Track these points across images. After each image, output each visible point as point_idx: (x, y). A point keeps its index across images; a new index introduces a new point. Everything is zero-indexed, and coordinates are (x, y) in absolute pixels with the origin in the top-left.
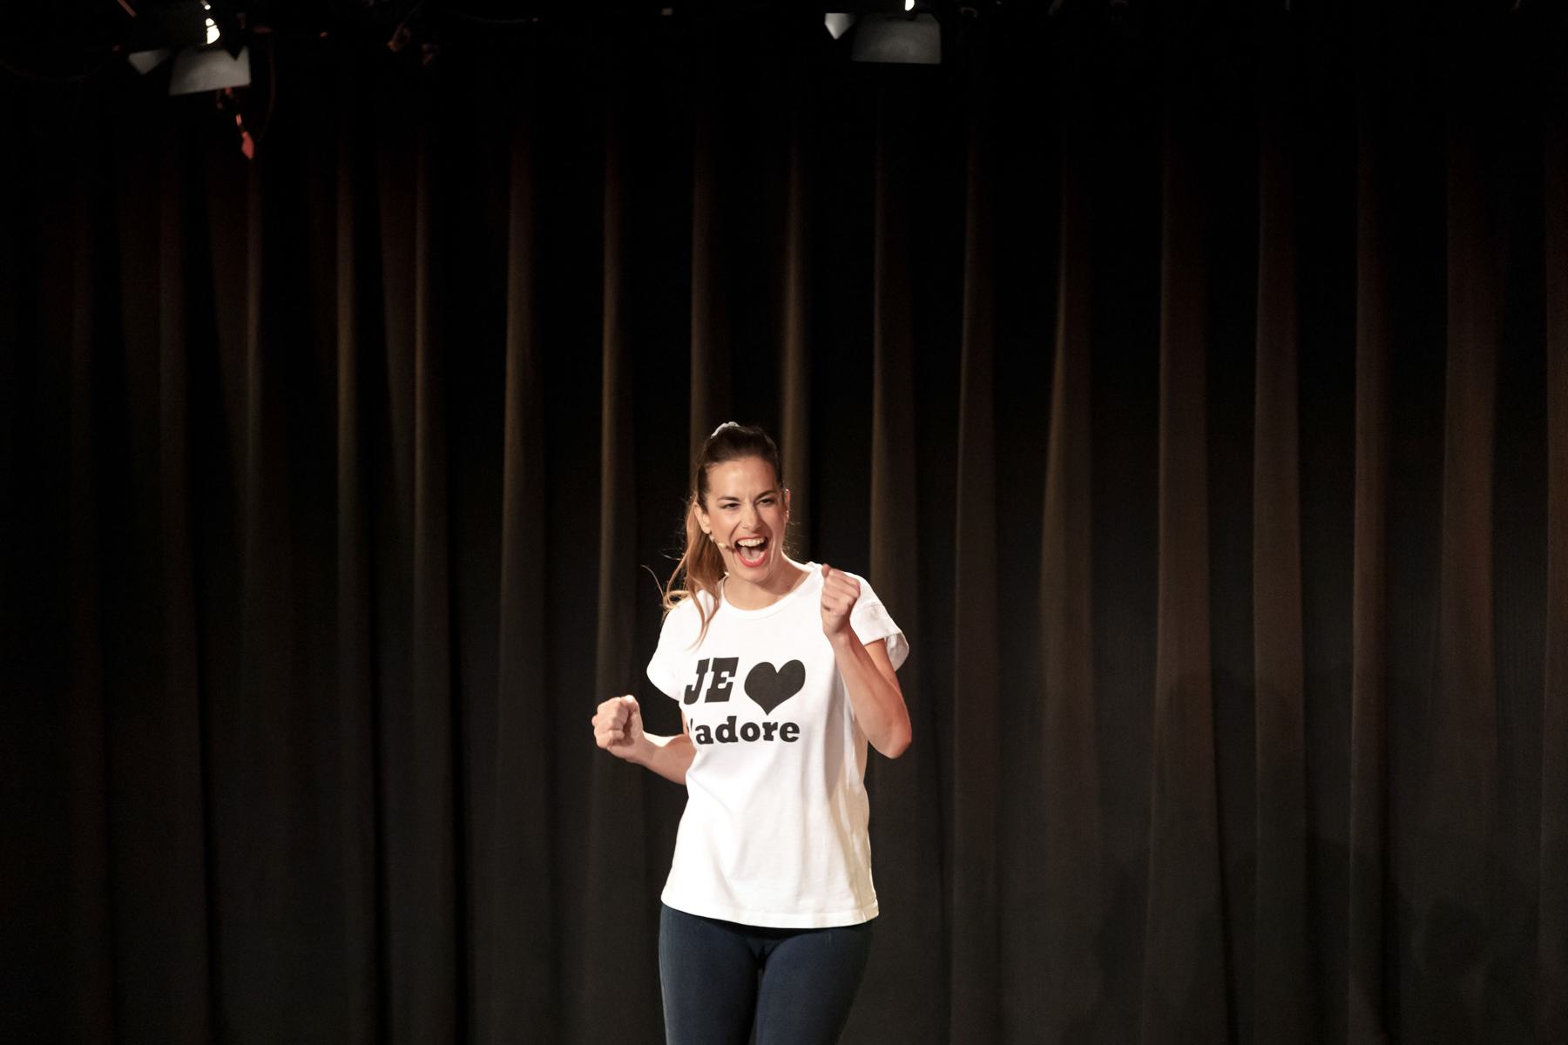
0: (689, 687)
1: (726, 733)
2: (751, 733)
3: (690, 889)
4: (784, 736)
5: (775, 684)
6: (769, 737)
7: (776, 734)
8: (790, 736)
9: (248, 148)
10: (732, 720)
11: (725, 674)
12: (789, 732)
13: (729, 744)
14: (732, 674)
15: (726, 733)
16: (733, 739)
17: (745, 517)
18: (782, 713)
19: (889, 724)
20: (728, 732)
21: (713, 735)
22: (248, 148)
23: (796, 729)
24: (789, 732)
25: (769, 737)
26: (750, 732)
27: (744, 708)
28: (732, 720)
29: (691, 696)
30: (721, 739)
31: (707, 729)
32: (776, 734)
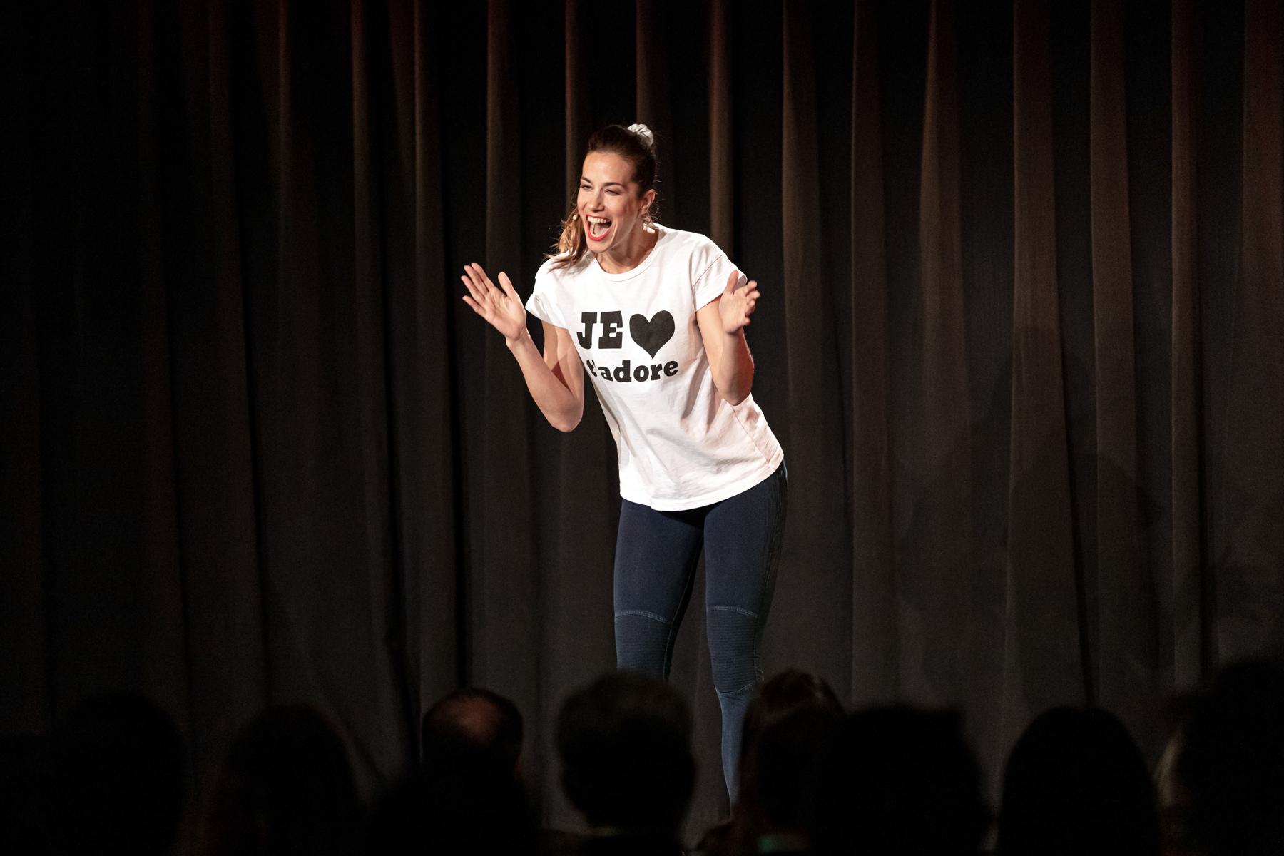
1: (622, 375)
2: (641, 374)
10: (627, 363)
11: (613, 325)
14: (620, 325)
15: (622, 375)
16: (627, 379)
17: (613, 204)
18: (664, 354)
20: (624, 373)
25: (655, 377)
28: (627, 363)
29: (586, 342)
31: (607, 371)
32: (661, 373)
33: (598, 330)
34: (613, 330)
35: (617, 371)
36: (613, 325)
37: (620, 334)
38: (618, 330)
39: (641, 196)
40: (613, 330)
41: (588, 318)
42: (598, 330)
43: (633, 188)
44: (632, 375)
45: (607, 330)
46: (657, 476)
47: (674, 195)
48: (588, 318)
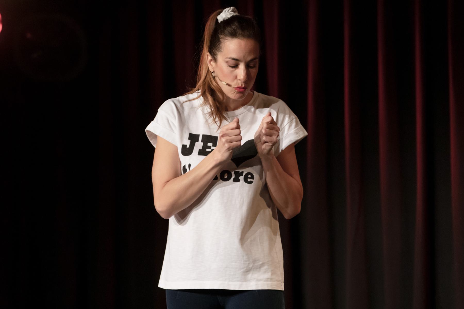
0: (184, 147)
4: (246, 180)
7: (241, 178)
8: (249, 180)
11: (210, 144)
14: (215, 145)
25: (236, 180)
29: (187, 151)
32: (241, 178)
33: (199, 145)
36: (210, 144)
38: (213, 148)
40: (210, 147)
42: (199, 145)
45: (205, 146)
46: (175, 275)
47: (261, 85)
48: (193, 138)
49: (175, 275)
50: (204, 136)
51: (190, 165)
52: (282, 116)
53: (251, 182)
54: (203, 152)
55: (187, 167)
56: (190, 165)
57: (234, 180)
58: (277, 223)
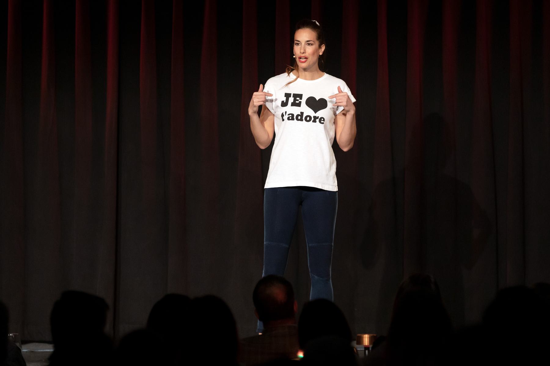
0: (283, 102)
1: (299, 118)
2: (308, 119)
3: (275, 180)
4: (320, 122)
5: (317, 104)
6: (314, 121)
7: (318, 120)
9: (317, 23)
10: (302, 113)
11: (298, 99)
12: (322, 120)
13: (299, 121)
14: (301, 99)
15: (299, 118)
16: (301, 120)
17: (310, 50)
18: (321, 113)
19: (333, 163)
21: (295, 117)
22: (317, 23)
23: (324, 120)
24: (322, 120)
25: (314, 121)
26: (308, 119)
27: (308, 111)
29: (284, 104)
30: (297, 119)
31: (293, 115)
32: (318, 120)
33: (291, 100)
34: (298, 100)
35: (298, 116)
36: (298, 99)
37: (300, 102)
39: (320, 47)
40: (298, 100)
41: (288, 96)
42: (291, 100)
43: (317, 43)
44: (304, 118)
46: (281, 175)
47: (328, 65)
48: (288, 96)
49: (281, 175)
50: (294, 94)
51: (286, 112)
52: (295, 77)
53: (323, 123)
54: (294, 104)
55: (284, 114)
56: (286, 112)
57: (313, 121)
58: (326, 76)
